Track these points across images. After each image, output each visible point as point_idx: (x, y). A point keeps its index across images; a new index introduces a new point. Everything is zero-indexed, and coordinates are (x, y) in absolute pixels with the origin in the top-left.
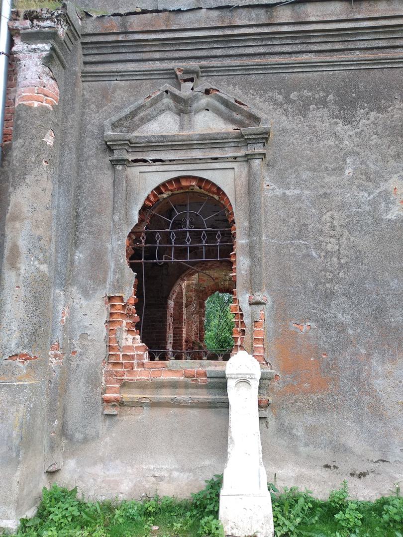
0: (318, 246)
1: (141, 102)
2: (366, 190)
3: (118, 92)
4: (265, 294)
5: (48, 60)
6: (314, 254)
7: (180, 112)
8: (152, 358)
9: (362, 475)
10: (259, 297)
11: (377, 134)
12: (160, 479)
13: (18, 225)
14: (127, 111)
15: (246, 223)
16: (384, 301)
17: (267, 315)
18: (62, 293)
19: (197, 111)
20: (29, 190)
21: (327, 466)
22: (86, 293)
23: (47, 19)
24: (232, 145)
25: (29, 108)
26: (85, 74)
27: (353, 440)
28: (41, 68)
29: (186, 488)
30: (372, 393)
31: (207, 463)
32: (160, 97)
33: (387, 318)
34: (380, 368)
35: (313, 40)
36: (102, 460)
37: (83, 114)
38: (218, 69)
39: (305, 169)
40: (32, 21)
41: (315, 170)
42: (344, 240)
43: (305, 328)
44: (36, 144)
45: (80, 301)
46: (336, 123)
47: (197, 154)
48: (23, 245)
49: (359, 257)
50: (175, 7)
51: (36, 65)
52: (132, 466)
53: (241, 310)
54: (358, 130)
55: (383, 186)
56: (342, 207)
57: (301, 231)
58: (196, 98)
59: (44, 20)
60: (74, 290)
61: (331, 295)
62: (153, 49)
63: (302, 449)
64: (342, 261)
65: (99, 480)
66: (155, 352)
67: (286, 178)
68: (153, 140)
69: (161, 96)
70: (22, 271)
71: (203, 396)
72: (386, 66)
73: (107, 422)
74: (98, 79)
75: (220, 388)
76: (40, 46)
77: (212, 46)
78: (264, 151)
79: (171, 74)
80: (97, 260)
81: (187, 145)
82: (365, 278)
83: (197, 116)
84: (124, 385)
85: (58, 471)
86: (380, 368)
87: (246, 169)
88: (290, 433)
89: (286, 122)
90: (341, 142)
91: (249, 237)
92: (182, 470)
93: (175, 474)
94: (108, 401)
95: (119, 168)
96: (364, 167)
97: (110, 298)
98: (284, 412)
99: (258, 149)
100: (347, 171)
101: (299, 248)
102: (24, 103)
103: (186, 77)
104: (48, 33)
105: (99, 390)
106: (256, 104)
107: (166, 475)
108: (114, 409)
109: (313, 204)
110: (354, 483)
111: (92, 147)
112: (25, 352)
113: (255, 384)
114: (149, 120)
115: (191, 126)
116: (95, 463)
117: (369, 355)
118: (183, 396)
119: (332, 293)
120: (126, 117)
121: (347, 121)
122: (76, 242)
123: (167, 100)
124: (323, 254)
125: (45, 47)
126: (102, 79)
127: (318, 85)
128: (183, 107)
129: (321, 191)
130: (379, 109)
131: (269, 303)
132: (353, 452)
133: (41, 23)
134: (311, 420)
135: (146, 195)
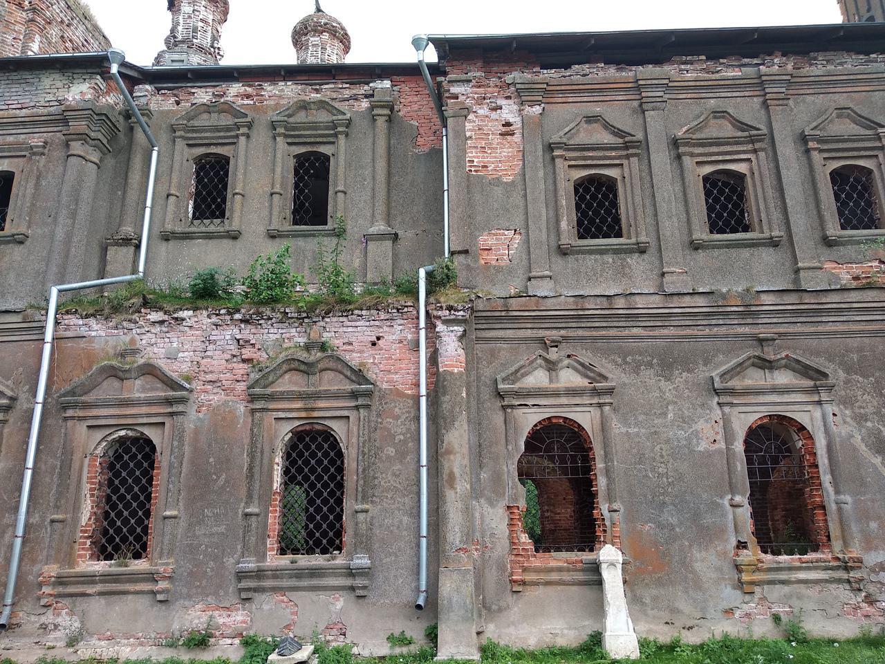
0: (653, 470)
1: (522, 363)
2: (683, 430)
3: (502, 352)
6: (651, 476)
7: (549, 370)
8: (537, 550)
9: (690, 628)
10: (615, 506)
11: (688, 389)
12: (556, 635)
13: (452, 457)
15: (602, 452)
16: (699, 508)
18: (477, 504)
20: (457, 432)
21: (667, 623)
22: (491, 504)
23: (461, 310)
24: (589, 394)
25: (452, 373)
27: (683, 605)
28: (457, 344)
29: (574, 640)
30: (693, 572)
31: (587, 623)
32: (536, 359)
33: (701, 520)
34: (698, 555)
35: (640, 319)
36: (513, 623)
37: (478, 368)
38: (574, 338)
39: (641, 414)
40: (450, 311)
41: (647, 414)
42: (670, 465)
43: (647, 528)
44: (458, 399)
45: (487, 509)
46: (660, 380)
47: (564, 400)
48: (457, 471)
49: (681, 478)
50: (543, 294)
52: (535, 627)
53: (602, 515)
54: (676, 386)
55: (695, 427)
56: (667, 441)
57: (641, 459)
58: (561, 360)
60: (482, 501)
62: (526, 321)
63: (650, 612)
64: (670, 480)
65: (513, 638)
66: (585, 546)
67: (628, 419)
69: (536, 359)
70: (458, 490)
71: (580, 576)
72: (692, 340)
73: (515, 596)
74: (487, 342)
75: (594, 571)
76: (456, 328)
77: (569, 320)
78: (611, 401)
79: (542, 341)
80: (497, 479)
81: (556, 394)
82: (685, 492)
84: (525, 570)
85: (481, 632)
86: (698, 555)
87: (600, 413)
88: (641, 601)
89: (625, 379)
90: (664, 393)
91: (605, 462)
92: (570, 628)
93: (566, 631)
94: (515, 581)
95: (509, 410)
96: (680, 413)
97: (509, 507)
98: (636, 587)
99: (607, 399)
100: (669, 416)
101: (640, 470)
102: (448, 369)
103: (553, 344)
105: (506, 574)
106: (604, 366)
107: (559, 632)
109: (648, 439)
110: (685, 633)
111: (486, 393)
112: (465, 547)
113: (619, 566)
115: (558, 381)
116: (509, 626)
117: (690, 546)
118: (566, 577)
119: (664, 503)
120: (512, 374)
121: (668, 379)
122: (480, 466)
123: (539, 361)
124: (656, 475)
125: (459, 329)
127: (646, 351)
128: (551, 366)
130: (689, 371)
131: (622, 510)
132: (683, 613)
133: (456, 313)
134: (654, 592)
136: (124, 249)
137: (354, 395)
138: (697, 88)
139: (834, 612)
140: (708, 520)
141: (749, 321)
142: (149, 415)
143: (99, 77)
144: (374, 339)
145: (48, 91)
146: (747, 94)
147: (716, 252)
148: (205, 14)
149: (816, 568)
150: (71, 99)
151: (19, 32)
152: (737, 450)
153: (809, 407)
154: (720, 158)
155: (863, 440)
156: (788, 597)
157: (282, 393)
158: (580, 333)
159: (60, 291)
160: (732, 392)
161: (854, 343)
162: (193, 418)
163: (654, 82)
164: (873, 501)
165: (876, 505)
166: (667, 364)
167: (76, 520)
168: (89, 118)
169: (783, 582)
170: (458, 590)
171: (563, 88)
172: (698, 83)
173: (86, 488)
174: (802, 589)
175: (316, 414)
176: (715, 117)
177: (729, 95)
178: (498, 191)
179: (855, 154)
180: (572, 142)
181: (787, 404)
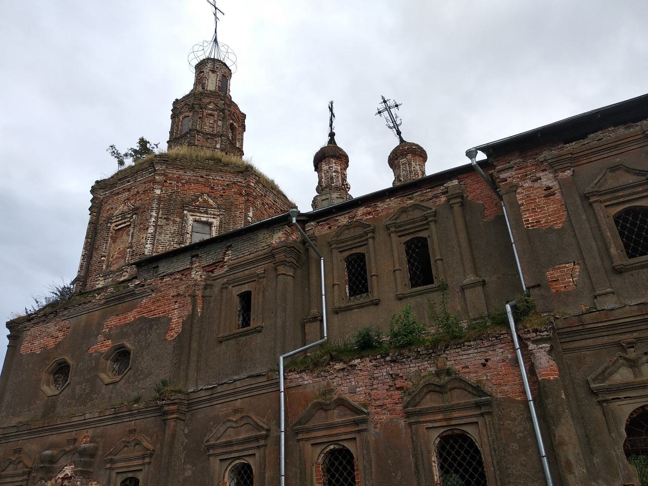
1: (606, 364)
7: (631, 367)
13: (565, 448)
14: (600, 370)
19: (643, 364)
25: (549, 381)
26: (565, 350)
28: (547, 357)
40: (536, 333)
51: (544, 356)
59: (543, 332)
60: (600, 481)
68: (620, 385)
76: (544, 345)
83: (643, 367)
104: (545, 338)
114: (613, 374)
120: (600, 374)
123: (621, 361)
125: (547, 346)
126: (575, 351)
133: (541, 334)
135: (626, 419)
136: (314, 324)
142: (345, 433)
143: (286, 226)
144: (483, 361)
145: (262, 241)
148: (336, 167)
150: (274, 243)
157: (427, 409)
162: (373, 433)
175: (453, 422)
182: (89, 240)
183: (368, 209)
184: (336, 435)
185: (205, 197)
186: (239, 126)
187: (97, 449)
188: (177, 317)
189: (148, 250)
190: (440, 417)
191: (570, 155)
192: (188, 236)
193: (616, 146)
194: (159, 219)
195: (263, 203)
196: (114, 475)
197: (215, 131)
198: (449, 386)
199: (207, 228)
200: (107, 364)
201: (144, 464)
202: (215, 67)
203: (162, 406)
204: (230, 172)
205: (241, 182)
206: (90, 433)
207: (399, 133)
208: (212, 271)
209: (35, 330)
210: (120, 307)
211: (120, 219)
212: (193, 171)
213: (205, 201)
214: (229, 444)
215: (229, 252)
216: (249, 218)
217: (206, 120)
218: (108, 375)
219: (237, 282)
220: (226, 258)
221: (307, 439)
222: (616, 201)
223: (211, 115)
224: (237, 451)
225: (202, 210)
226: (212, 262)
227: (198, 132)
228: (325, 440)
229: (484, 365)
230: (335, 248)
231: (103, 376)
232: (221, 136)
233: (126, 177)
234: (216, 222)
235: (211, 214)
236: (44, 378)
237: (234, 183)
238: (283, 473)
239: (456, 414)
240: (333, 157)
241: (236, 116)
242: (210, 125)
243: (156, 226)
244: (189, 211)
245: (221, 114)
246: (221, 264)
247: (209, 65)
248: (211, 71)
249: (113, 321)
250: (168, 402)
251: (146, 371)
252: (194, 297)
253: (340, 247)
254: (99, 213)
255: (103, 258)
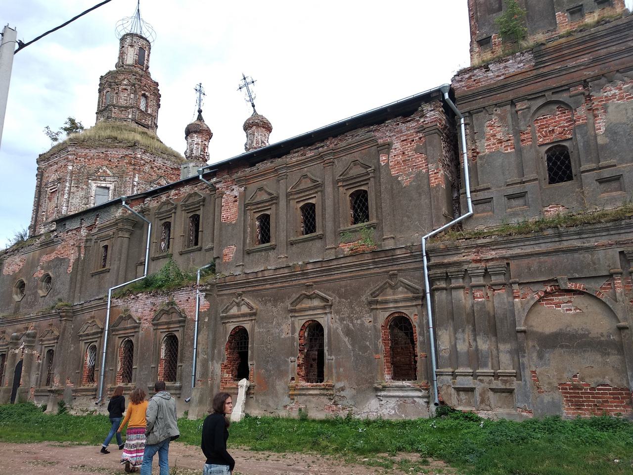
4: (254, 362)
5: (206, 297)
17: (254, 367)
27: (271, 403)
38: (246, 292)
47: (241, 319)
55: (282, 327)
56: (272, 334)
61: (268, 361)
63: (260, 406)
108: (313, 418)
128: (238, 305)
129: (268, 329)
130: (283, 302)
134: (262, 398)
136: (141, 267)
137: (180, 322)
138: (299, 164)
139: (321, 408)
140: (283, 368)
141: (305, 277)
142: (131, 333)
144: (187, 299)
146: (318, 162)
147: (300, 245)
148: (197, 140)
149: (316, 389)
151: (131, 175)
152: (296, 337)
153: (323, 316)
154: (305, 198)
155: (342, 330)
156: (306, 401)
157: (161, 322)
158: (250, 289)
159: (112, 290)
160: (295, 311)
161: (343, 283)
162: (141, 333)
163: (281, 167)
164: (342, 358)
165: (344, 360)
166: (276, 299)
167: (116, 369)
168: (122, 222)
169: (304, 395)
170: (196, 396)
171: (251, 176)
172: (298, 163)
173: (119, 358)
174: (311, 398)
175: (170, 330)
176: (304, 178)
177: (311, 164)
178: (230, 228)
179: (359, 184)
180: (253, 202)
181: (315, 314)
182: (36, 199)
183: (176, 191)
184: (128, 333)
185: (104, 168)
186: (151, 95)
187: (36, 333)
188: (72, 258)
189: (64, 211)
190: (166, 327)
191: (244, 178)
192: (92, 198)
193: (264, 174)
194: (72, 188)
195: (152, 167)
196: (43, 348)
197: (128, 104)
198: (171, 311)
199: (107, 191)
200: (42, 284)
201: (54, 343)
202: (133, 41)
203: (59, 313)
204: (123, 148)
205: (131, 154)
206: (34, 324)
207: (253, 106)
208: (91, 230)
209: (9, 260)
210: (48, 249)
211: (52, 185)
212: (96, 149)
213: (104, 171)
214: (87, 335)
215: (98, 219)
216: (134, 183)
217: (121, 94)
218: (43, 291)
219: (103, 239)
220: (97, 222)
221: (117, 335)
222: (257, 210)
223: (126, 89)
224: (90, 339)
225: (102, 178)
226: (90, 224)
227: (114, 106)
228: (123, 335)
229: (188, 300)
230: (157, 217)
231: (40, 291)
232: (132, 107)
233: (54, 154)
234: (112, 187)
235: (108, 181)
236: (14, 291)
237: (126, 155)
238: (105, 351)
239: (172, 326)
240: (195, 132)
241: (147, 86)
242: (125, 98)
243: (69, 193)
244: (93, 180)
245: (133, 87)
246: (94, 226)
247: (128, 40)
248: (130, 45)
249: (45, 258)
250: (61, 311)
251: (58, 291)
252: (79, 247)
253: (160, 217)
254: (41, 179)
255: (43, 213)
